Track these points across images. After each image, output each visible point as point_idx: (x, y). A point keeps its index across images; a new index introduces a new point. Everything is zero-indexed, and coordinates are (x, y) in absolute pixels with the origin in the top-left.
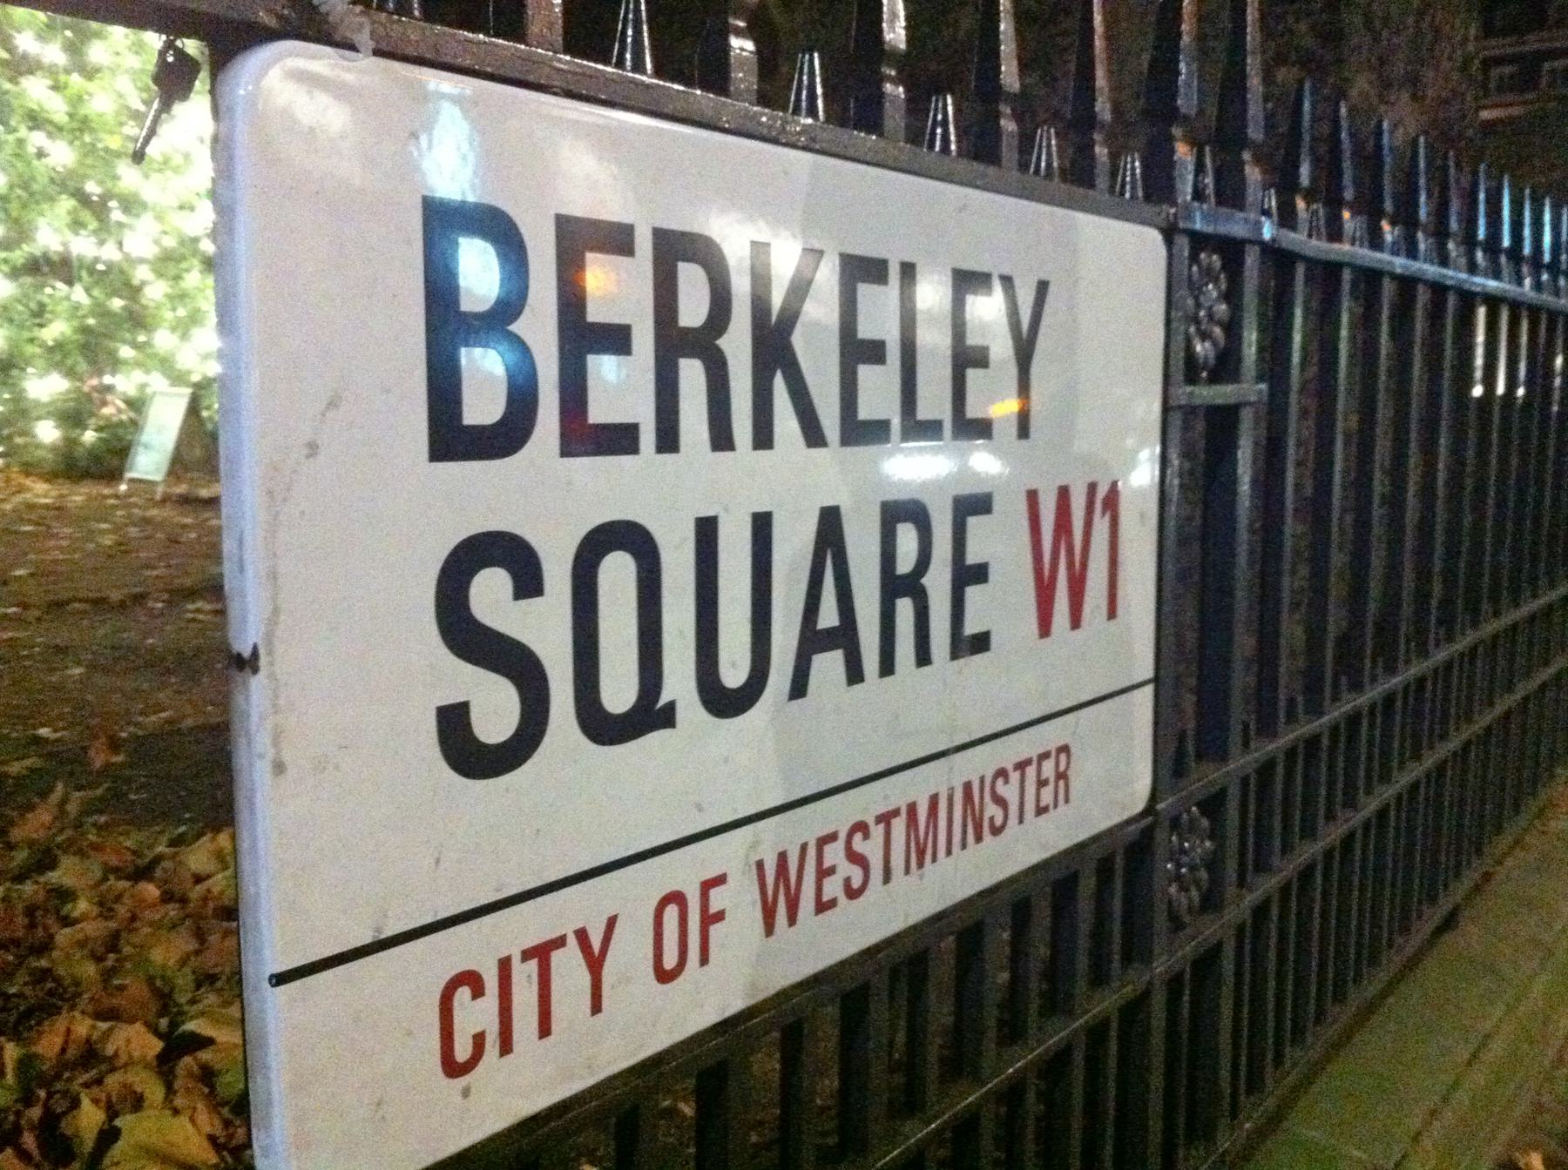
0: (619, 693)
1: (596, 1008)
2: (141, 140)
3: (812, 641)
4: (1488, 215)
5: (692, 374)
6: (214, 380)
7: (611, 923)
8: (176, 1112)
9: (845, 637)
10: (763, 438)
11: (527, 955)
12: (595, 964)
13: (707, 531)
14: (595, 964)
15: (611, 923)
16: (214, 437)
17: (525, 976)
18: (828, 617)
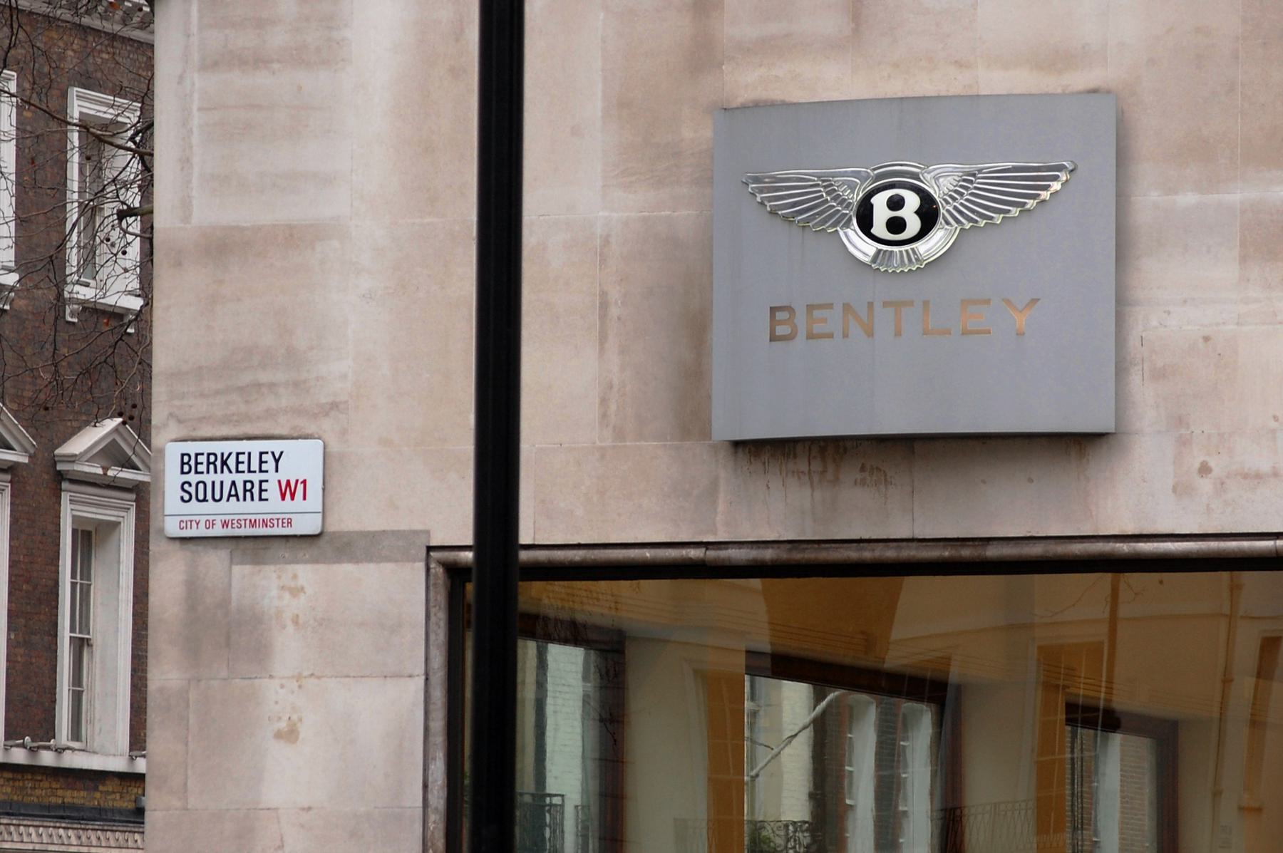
0: (201, 497)
1: (277, 471)
2: (114, 484)
3: (230, 495)
4: (806, 189)
5: (212, 467)
6: (109, 418)
7: (282, 453)
8: (31, 334)
9: (236, 495)
10: (222, 472)
11: (207, 501)
12: (277, 461)
13: (213, 483)
14: (198, 524)
15: (282, 453)
16: (67, 219)
17: (189, 523)
18: (233, 492)
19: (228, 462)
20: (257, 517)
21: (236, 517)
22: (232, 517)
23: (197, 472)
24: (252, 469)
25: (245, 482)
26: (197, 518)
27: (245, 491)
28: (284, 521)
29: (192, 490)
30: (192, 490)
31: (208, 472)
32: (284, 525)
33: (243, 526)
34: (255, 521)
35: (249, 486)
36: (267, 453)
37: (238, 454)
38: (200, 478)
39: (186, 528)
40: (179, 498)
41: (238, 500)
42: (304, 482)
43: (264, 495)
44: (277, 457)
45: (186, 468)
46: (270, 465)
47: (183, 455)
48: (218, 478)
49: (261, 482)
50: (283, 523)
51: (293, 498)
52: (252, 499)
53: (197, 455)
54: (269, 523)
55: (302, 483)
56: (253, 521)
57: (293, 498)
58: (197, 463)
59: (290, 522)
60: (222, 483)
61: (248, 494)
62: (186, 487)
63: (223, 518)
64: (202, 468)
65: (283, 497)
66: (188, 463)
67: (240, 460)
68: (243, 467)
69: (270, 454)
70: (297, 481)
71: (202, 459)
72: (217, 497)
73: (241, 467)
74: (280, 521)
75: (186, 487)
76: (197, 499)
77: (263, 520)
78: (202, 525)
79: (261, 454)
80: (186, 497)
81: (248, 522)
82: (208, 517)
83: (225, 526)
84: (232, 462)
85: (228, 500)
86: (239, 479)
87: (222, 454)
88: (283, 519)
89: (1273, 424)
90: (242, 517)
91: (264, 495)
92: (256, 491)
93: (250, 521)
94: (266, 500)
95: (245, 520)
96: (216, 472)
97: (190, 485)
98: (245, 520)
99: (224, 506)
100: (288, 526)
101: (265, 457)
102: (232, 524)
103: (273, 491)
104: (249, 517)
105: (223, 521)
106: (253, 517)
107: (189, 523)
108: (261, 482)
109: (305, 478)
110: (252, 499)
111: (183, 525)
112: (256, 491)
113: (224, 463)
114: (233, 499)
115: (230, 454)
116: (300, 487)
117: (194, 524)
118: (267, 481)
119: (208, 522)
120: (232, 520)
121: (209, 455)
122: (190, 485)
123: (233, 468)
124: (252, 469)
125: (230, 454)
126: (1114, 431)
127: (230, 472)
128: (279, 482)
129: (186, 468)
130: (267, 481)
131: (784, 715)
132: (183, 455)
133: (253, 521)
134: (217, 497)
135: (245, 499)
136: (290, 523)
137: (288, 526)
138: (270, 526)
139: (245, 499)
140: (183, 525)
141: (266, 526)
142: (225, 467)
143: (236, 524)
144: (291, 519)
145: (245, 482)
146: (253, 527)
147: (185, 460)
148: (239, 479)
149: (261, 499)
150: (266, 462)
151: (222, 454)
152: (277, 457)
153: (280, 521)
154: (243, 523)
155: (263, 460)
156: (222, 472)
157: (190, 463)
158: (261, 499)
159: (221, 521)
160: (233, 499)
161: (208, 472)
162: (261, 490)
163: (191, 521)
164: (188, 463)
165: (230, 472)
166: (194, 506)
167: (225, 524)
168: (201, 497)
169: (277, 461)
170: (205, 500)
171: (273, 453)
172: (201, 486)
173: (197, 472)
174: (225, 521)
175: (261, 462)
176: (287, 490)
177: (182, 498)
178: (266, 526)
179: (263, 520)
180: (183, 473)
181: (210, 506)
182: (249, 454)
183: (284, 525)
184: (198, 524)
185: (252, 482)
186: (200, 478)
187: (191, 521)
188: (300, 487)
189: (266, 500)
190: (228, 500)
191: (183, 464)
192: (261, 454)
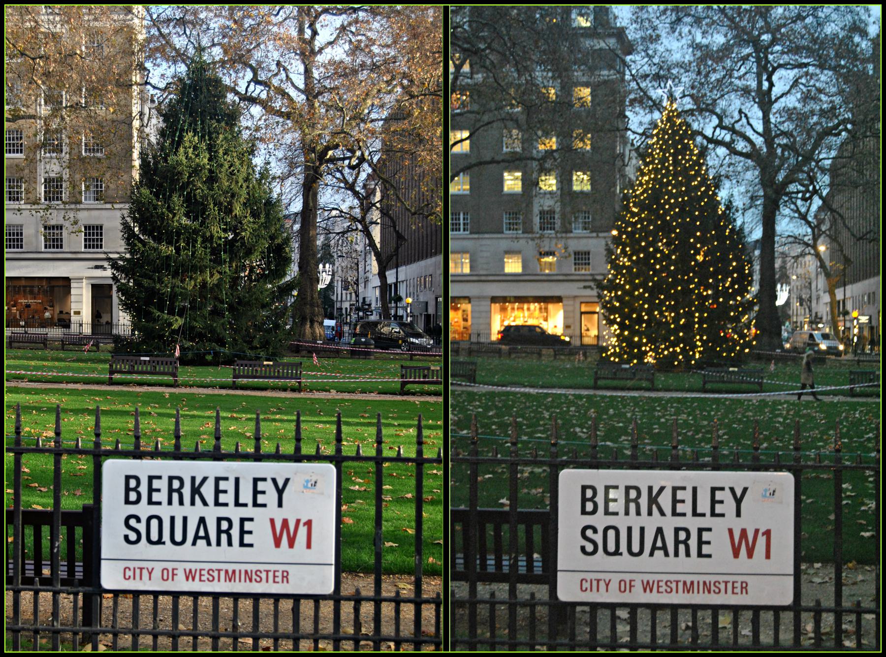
0: (611, 547)
1: (280, 505)
5: (175, 496)
11: (164, 543)
18: (659, 544)
19: (203, 490)
20: (237, 567)
21: (665, 577)
22: (202, 566)
23: (150, 502)
24: (699, 511)
25: (677, 530)
26: (150, 565)
27: (219, 532)
28: (277, 574)
29: (142, 527)
30: (142, 527)
32: (277, 579)
33: (674, 590)
35: (225, 525)
37: (218, 480)
38: (154, 510)
39: (134, 578)
40: (122, 538)
42: (768, 533)
43: (247, 539)
45: (133, 496)
46: (728, 506)
47: (128, 478)
50: (275, 576)
52: (230, 544)
53: (151, 479)
55: (305, 524)
56: (230, 573)
58: (151, 490)
60: (185, 519)
62: (133, 522)
63: (188, 566)
65: (736, 554)
66: (135, 489)
67: (679, 497)
71: (162, 484)
72: (178, 537)
74: (271, 575)
76: (149, 540)
77: (705, 583)
78: (614, 586)
81: (681, 585)
83: (648, 590)
85: (194, 543)
87: (650, 489)
88: (733, 583)
93: (227, 572)
95: (677, 582)
96: (638, 513)
97: (138, 520)
98: (726, 583)
100: (742, 593)
101: (719, 495)
102: (658, 587)
103: (261, 533)
104: (682, 578)
105: (188, 571)
106: (230, 567)
108: (700, 531)
109: (769, 528)
110: (230, 544)
111: (129, 573)
112: (693, 543)
114: (201, 543)
116: (761, 541)
119: (165, 572)
120: (658, 582)
122: (595, 531)
123: (210, 499)
124: (699, 511)
127: (662, 514)
128: (272, 521)
132: (584, 488)
133: (230, 573)
136: (287, 577)
137: (742, 593)
138: (256, 580)
140: (586, 585)
142: (654, 507)
143: (665, 587)
144: (287, 572)
145: (677, 530)
146: (230, 580)
148: (211, 514)
157: (139, 489)
158: (700, 555)
159: (643, 582)
160: (201, 543)
165: (662, 514)
168: (611, 547)
173: (150, 502)
175: (714, 502)
178: (709, 592)
179: (246, 572)
180: (584, 512)
181: (625, 561)
183: (277, 579)
185: (229, 520)
186: (154, 510)
187: (598, 581)
188: (761, 541)
189: (251, 545)
190: (194, 543)
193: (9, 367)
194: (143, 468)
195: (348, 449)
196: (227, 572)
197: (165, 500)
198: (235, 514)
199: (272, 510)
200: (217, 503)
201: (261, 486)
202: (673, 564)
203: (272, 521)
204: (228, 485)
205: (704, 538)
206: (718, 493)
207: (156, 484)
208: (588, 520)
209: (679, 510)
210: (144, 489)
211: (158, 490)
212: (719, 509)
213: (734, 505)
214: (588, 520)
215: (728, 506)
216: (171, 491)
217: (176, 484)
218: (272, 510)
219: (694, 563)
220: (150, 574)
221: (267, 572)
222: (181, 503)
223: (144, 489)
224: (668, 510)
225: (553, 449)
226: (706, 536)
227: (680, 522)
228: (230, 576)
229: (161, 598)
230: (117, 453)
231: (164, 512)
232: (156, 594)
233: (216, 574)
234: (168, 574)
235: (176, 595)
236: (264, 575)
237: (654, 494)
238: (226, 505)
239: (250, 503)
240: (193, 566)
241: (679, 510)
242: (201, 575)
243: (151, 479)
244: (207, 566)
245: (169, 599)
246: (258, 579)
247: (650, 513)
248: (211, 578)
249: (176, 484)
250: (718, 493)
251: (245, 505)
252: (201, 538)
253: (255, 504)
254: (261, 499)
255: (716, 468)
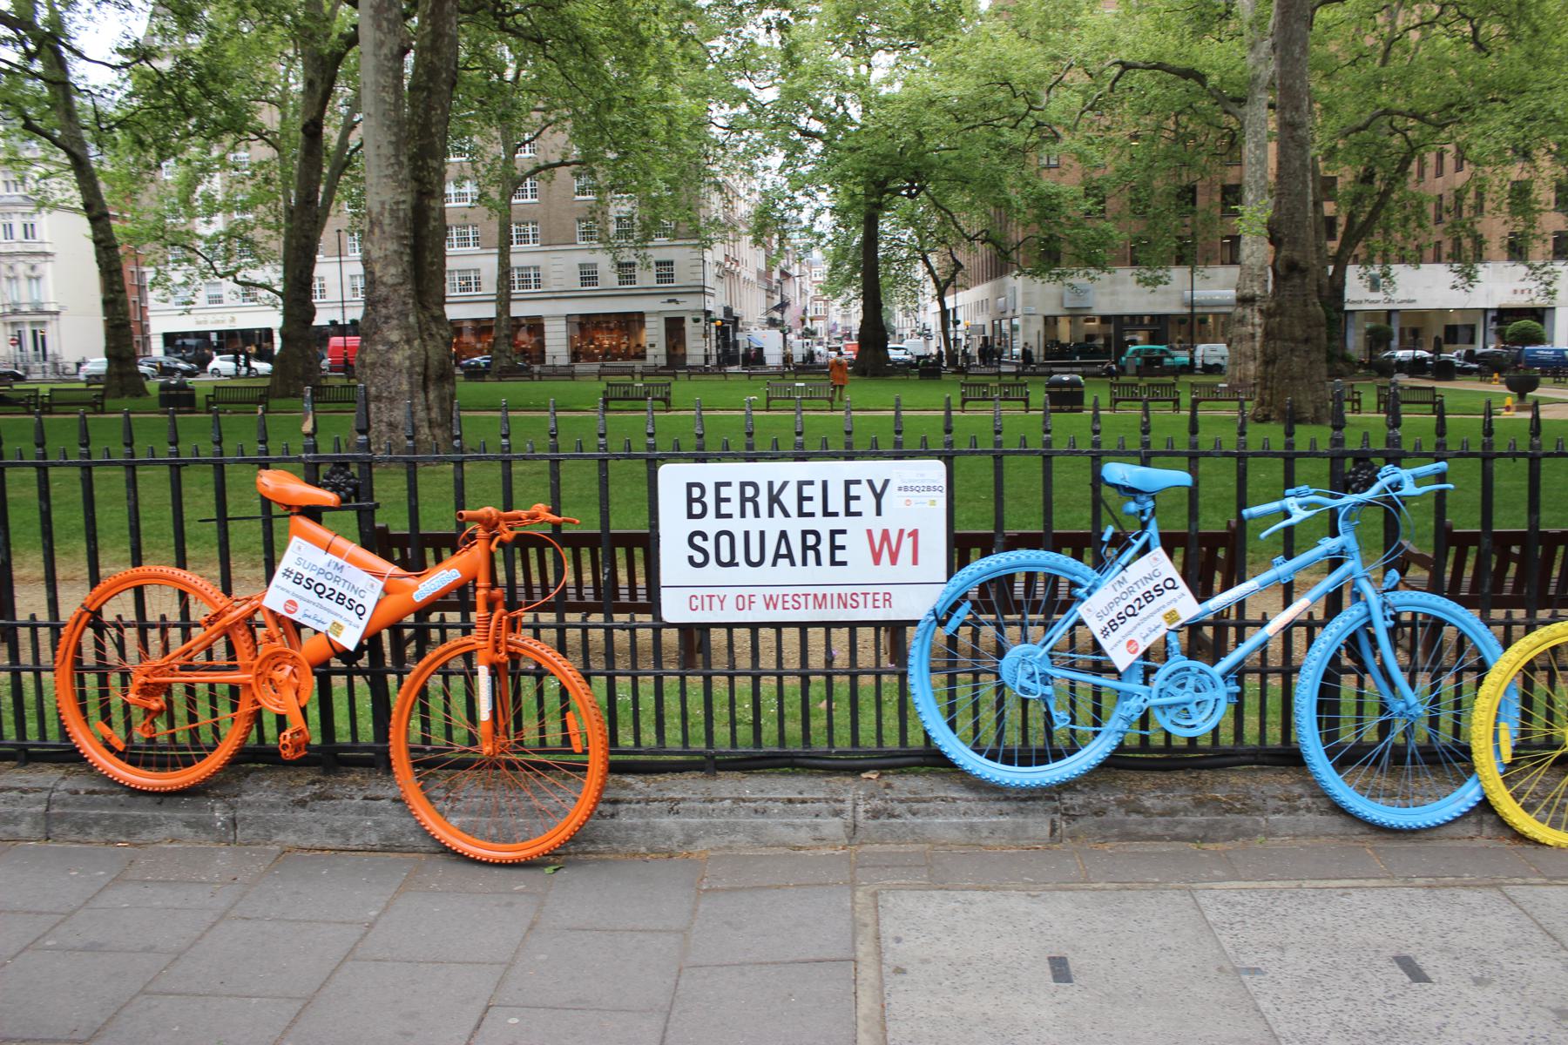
0: (725, 557)
1: (879, 513)
3: (777, 556)
5: (749, 506)
7: (886, 482)
9: (789, 556)
11: (737, 564)
12: (878, 497)
13: (747, 534)
15: (886, 482)
18: (783, 551)
21: (791, 591)
23: (719, 515)
24: (830, 510)
25: (805, 533)
27: (805, 548)
29: (709, 546)
30: (709, 546)
31: (743, 515)
32: (877, 604)
34: (824, 596)
35: (811, 540)
36: (858, 482)
37: (801, 484)
38: (724, 524)
41: (793, 564)
42: (914, 534)
43: (840, 555)
44: (878, 491)
45: (697, 509)
46: (866, 503)
47: (690, 486)
48: (753, 525)
49: (833, 533)
51: (894, 561)
52: (818, 563)
53: (718, 485)
54: (849, 601)
55: (910, 535)
56: (820, 598)
57: (894, 561)
58: (719, 500)
59: (888, 599)
60: (762, 534)
61: (811, 554)
62: (698, 540)
63: (768, 591)
64: (732, 507)
65: (877, 559)
66: (699, 500)
68: (814, 506)
69: (865, 484)
70: (901, 532)
71: (732, 492)
72: (755, 557)
73: (807, 506)
74: (870, 598)
75: (698, 540)
77: (839, 595)
79: (848, 484)
80: (699, 558)
81: (811, 599)
82: (768, 591)
83: (771, 606)
84: (789, 498)
85: (774, 564)
86: (795, 526)
87: (771, 484)
89: (602, 441)
90: (800, 590)
91: (840, 555)
92: (824, 548)
93: (815, 596)
94: (844, 563)
99: (766, 573)
101: (854, 490)
103: (856, 547)
106: (820, 591)
107: (707, 600)
108: (833, 533)
110: (818, 563)
111: (696, 603)
112: (824, 548)
113: (774, 499)
115: (785, 484)
116: (907, 543)
117: (716, 601)
118: (843, 532)
121: (743, 485)
122: (705, 538)
124: (830, 510)
125: (785, 484)
126: (1121, 668)
127: (786, 514)
128: (869, 532)
129: (697, 509)
130: (843, 532)
131: (1418, 962)
132: (690, 486)
133: (820, 598)
134: (755, 557)
135: (805, 563)
139: (805, 563)
140: (696, 603)
141: (845, 606)
142: (776, 506)
145: (805, 533)
146: (820, 607)
147: (693, 496)
149: (833, 563)
150: (857, 498)
151: (771, 484)
152: (878, 491)
153: (870, 598)
154: (802, 600)
155: (805, 494)
156: (771, 514)
158: (833, 563)
161: (743, 515)
162: (834, 548)
163: (711, 597)
164: (699, 500)
165: (786, 514)
166: (712, 572)
167: (770, 603)
168: (725, 557)
169: (878, 497)
170: (732, 563)
171: (870, 482)
172: (725, 540)
173: (719, 515)
174: (771, 597)
175: (849, 498)
176: (884, 548)
177: (691, 559)
178: (845, 606)
179: (839, 595)
180: (691, 516)
181: (743, 573)
182: (825, 484)
183: (877, 604)
184: (722, 602)
186: (724, 524)
188: (907, 543)
189: (844, 563)
190: (774, 564)
191: (690, 500)
192: (848, 484)
193: (1485, 346)
194: (708, 473)
195: (1205, 440)
196: (815, 596)
197: (736, 511)
198: (824, 525)
199: (869, 519)
200: (801, 514)
201: (854, 490)
202: (799, 574)
203: (869, 532)
204: (814, 491)
205: (838, 543)
206: (853, 487)
207: (725, 492)
208: (697, 525)
209: (806, 510)
210: (710, 499)
211: (728, 500)
212: (854, 506)
213: (873, 501)
214: (697, 525)
215: (866, 503)
216: (744, 500)
217: (750, 492)
218: (869, 519)
219: (827, 572)
220: (722, 602)
221: (865, 594)
222: (757, 515)
223: (710, 499)
224: (793, 510)
225: (651, 440)
226: (839, 540)
227: (808, 524)
228: (820, 602)
229: (735, 630)
230: (677, 456)
231: (737, 526)
232: (730, 626)
233: (802, 600)
234: (745, 603)
235: (754, 627)
236: (861, 599)
237: (775, 492)
238: (812, 515)
239: (842, 511)
240: (775, 591)
241: (806, 510)
242: (784, 602)
243: (718, 485)
244: (791, 591)
245: (796, 631)
246: (855, 604)
247: (771, 514)
248: (796, 605)
249: (750, 492)
250: (853, 487)
251: (836, 514)
252: (783, 556)
253: (848, 513)
254: (854, 506)
255: (850, 457)
